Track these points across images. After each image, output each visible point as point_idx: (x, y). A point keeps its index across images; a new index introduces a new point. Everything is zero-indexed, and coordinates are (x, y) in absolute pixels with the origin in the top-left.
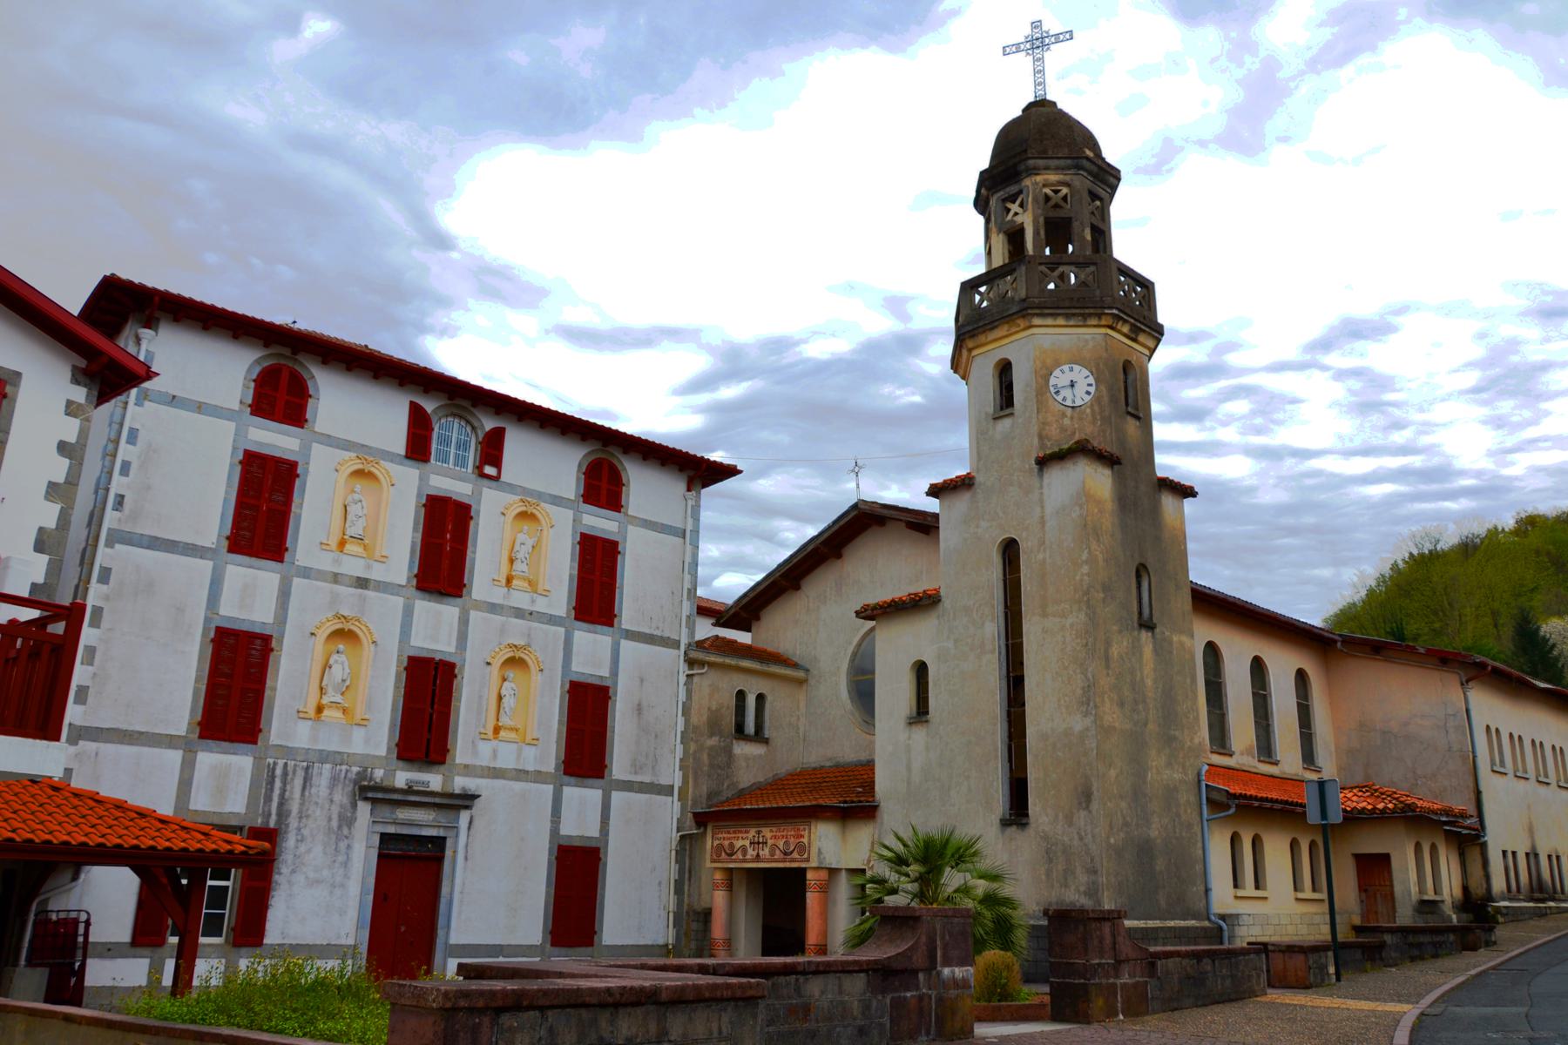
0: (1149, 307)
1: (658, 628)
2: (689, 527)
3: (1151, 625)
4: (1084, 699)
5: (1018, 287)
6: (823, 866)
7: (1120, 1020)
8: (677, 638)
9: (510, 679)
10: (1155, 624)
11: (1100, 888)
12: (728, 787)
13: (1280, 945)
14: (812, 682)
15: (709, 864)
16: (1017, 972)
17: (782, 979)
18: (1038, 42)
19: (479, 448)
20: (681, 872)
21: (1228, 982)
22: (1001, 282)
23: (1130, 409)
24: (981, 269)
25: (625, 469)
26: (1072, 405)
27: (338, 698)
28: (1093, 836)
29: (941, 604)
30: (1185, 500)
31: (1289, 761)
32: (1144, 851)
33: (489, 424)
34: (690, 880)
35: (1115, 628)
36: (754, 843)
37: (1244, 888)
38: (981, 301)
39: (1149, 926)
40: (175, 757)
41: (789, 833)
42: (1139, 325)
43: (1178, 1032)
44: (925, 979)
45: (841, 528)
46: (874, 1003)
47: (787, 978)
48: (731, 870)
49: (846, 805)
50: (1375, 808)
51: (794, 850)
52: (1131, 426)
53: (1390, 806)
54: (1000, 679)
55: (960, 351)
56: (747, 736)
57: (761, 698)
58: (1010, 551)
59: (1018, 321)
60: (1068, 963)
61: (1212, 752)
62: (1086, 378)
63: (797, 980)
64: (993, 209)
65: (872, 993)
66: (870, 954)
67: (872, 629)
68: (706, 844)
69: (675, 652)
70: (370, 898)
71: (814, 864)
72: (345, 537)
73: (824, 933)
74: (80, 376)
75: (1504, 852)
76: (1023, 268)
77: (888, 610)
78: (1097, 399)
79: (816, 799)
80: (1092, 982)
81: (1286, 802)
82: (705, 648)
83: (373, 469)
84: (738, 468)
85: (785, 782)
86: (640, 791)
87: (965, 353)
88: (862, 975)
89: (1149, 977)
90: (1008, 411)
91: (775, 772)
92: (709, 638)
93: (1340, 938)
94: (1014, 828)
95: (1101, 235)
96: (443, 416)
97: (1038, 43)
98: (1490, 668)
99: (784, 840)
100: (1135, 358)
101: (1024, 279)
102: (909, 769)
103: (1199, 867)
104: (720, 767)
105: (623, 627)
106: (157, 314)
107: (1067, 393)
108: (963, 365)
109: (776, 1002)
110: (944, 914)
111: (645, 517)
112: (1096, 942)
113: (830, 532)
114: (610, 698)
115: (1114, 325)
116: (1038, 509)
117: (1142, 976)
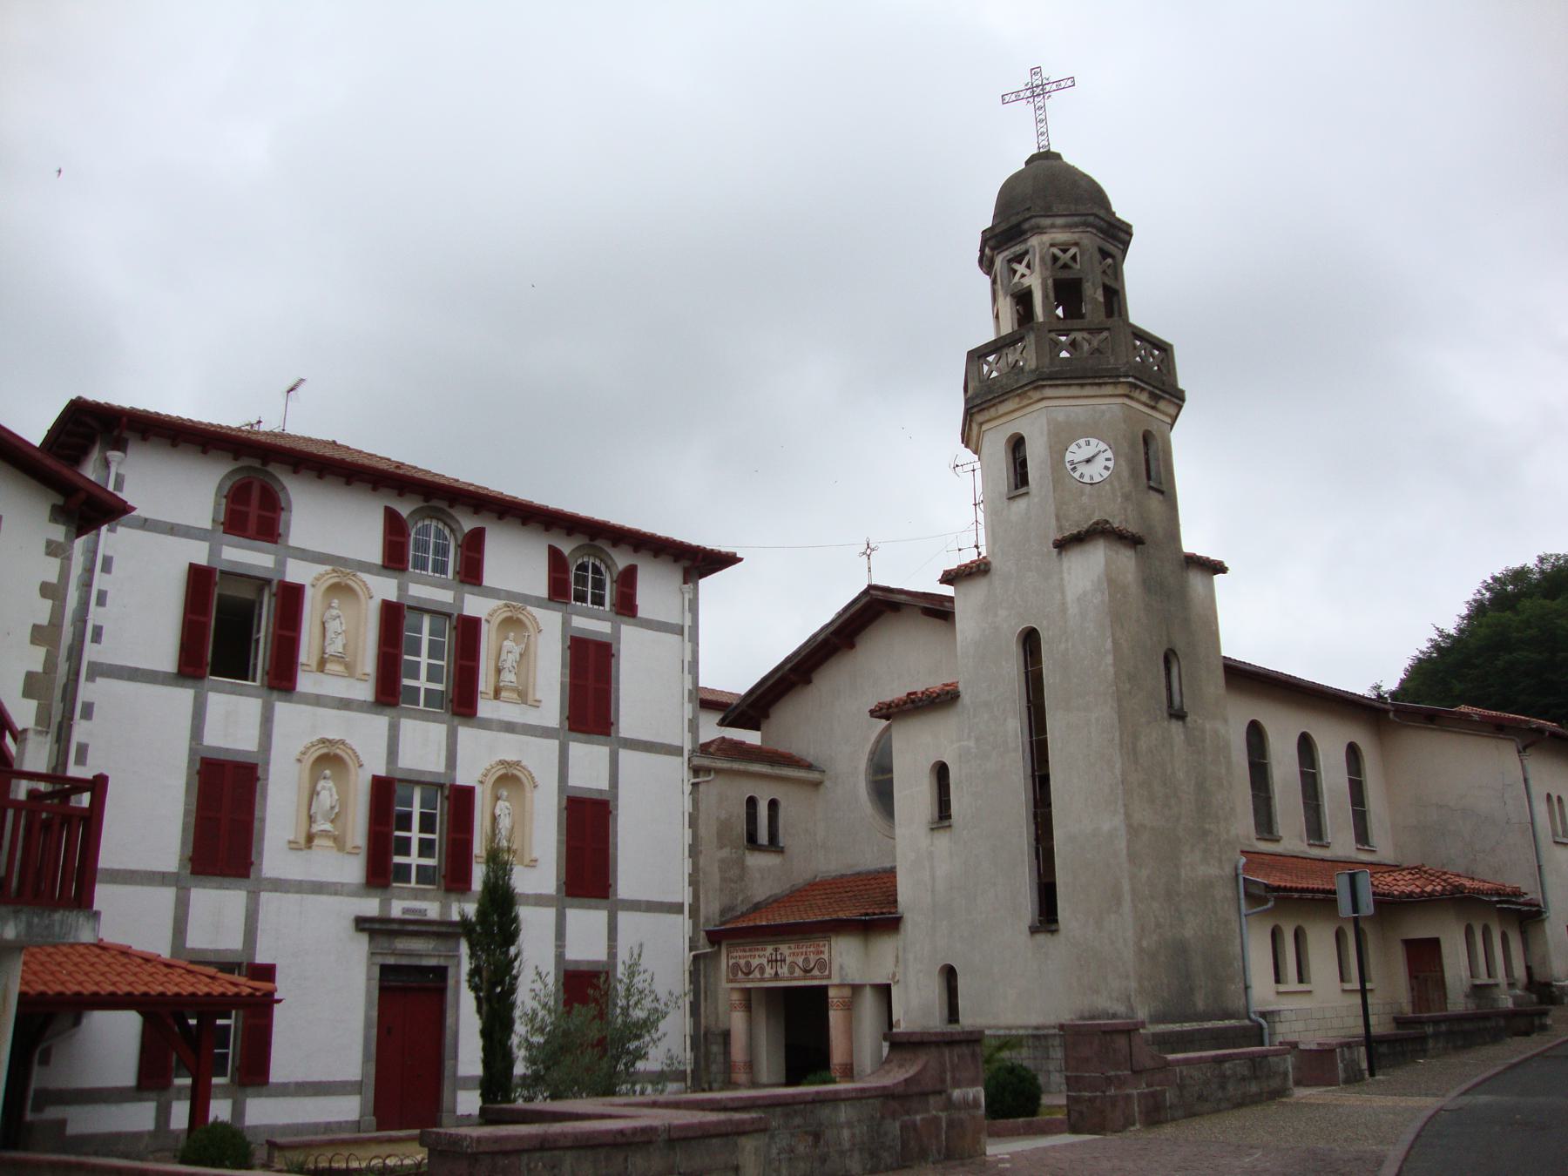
0: (1169, 372)
2: (688, 623)
5: (1027, 357)
6: (846, 982)
8: (680, 744)
9: (504, 797)
12: (742, 902)
14: (827, 783)
15: (725, 985)
18: (1038, 90)
19: (459, 553)
23: (1152, 484)
27: (328, 826)
29: (960, 700)
30: (1215, 577)
31: (1341, 843)
32: (1180, 949)
33: (468, 524)
34: (706, 1000)
36: (772, 961)
39: (1185, 1029)
40: (168, 895)
42: (1157, 392)
45: (852, 615)
48: (748, 990)
49: (867, 918)
50: (1422, 891)
51: (814, 968)
52: (1155, 501)
53: (1438, 888)
55: (970, 425)
57: (773, 805)
58: (1030, 641)
68: (720, 963)
69: (679, 759)
70: (374, 1032)
71: (835, 980)
72: (326, 656)
73: (851, 1053)
74: (59, 514)
78: (1115, 474)
83: (350, 582)
84: (738, 556)
87: (975, 427)
93: (1375, 1030)
95: (1114, 297)
96: (420, 519)
97: (1038, 91)
98: (1547, 734)
99: (803, 957)
100: (1155, 427)
101: (1033, 346)
102: (933, 878)
103: (1238, 964)
105: (621, 735)
106: (126, 434)
114: (610, 812)
116: (1059, 596)
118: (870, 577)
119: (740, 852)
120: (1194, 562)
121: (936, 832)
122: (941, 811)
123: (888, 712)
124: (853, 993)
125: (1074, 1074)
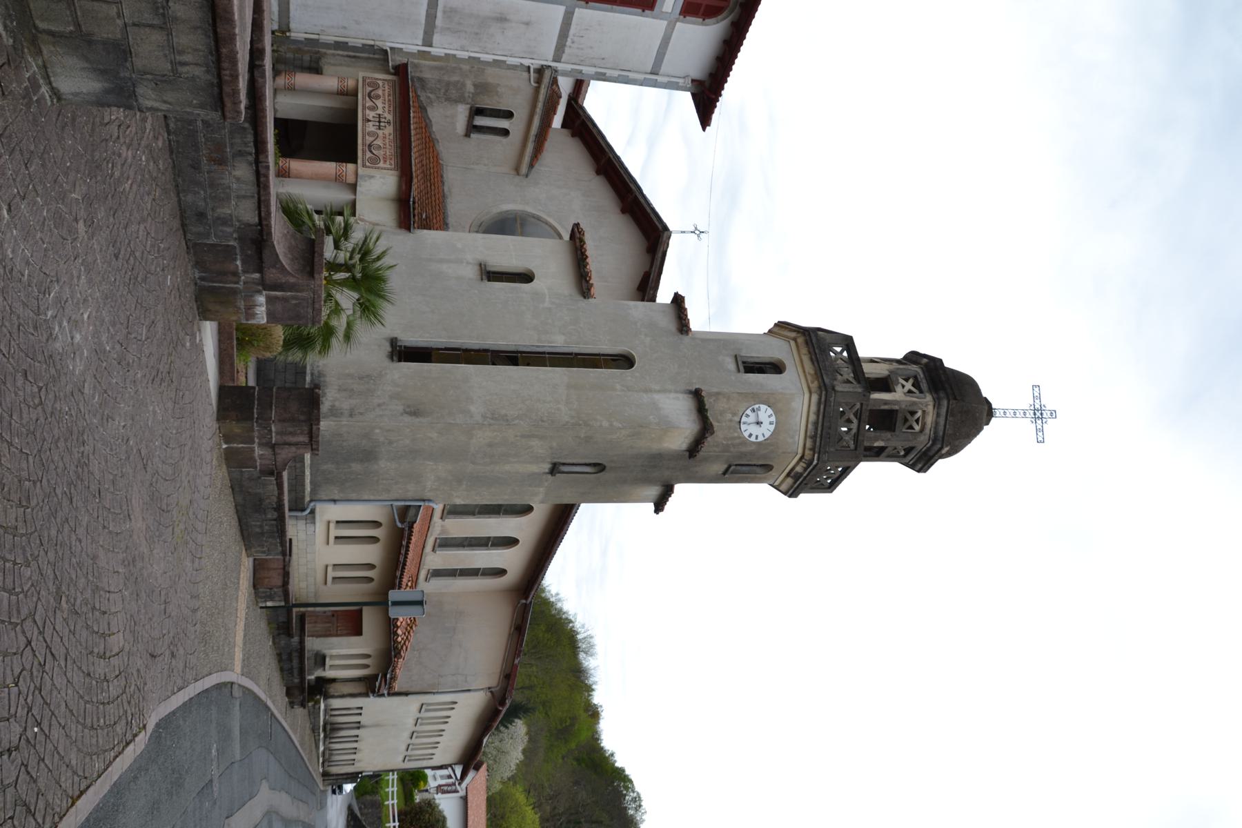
1: (573, 42)
2: (660, 79)
3: (555, 471)
4: (497, 416)
6: (359, 179)
7: (221, 445)
8: (562, 60)
10: (555, 475)
11: (338, 419)
12: (429, 98)
13: (289, 566)
14: (517, 179)
15: (361, 75)
16: (263, 356)
17: (250, 138)
20: (354, 49)
21: (258, 530)
22: (850, 370)
23: (732, 468)
24: (862, 353)
25: (718, 22)
26: (742, 421)
28: (381, 416)
29: (582, 298)
32: (369, 456)
34: (349, 56)
35: (554, 444)
36: (380, 117)
37: (336, 528)
38: (835, 353)
41: (388, 151)
42: (801, 480)
43: (211, 498)
44: (253, 279)
45: (649, 214)
46: (229, 230)
47: (252, 144)
48: (356, 95)
49: (411, 203)
50: (398, 627)
51: (373, 154)
52: (719, 468)
53: (399, 639)
54: (515, 345)
55: (795, 331)
56: (473, 118)
57: (505, 132)
58: (625, 361)
59: (816, 383)
60: (272, 403)
61: (445, 505)
62: (763, 434)
63: (251, 154)
64: (909, 367)
65: (239, 228)
66: (278, 227)
67: (560, 237)
69: (551, 57)
71: (361, 171)
73: (299, 176)
75: (361, 708)
76: (860, 390)
77: (579, 252)
78: (745, 442)
79: (417, 177)
80: (255, 424)
81: (404, 564)
82: (552, 85)
84: (708, 128)
85: (431, 150)
86: (428, 15)
87: (793, 335)
88: (257, 220)
89: (260, 470)
90: (741, 368)
91: (440, 141)
92: (559, 88)
94: (389, 349)
95: (877, 454)
98: (501, 708)
99: (382, 145)
101: (851, 390)
102: (441, 261)
103: (354, 496)
104: (447, 91)
105: (577, 9)
107: (752, 418)
108: (782, 333)
109: (227, 130)
110: (315, 300)
111: (672, 38)
112: (291, 429)
113: (645, 205)
115: (803, 460)
116: (657, 387)
117: (260, 465)
118: (677, 232)
119: (470, 100)
120: (667, 491)
121: (478, 267)
122: (495, 273)
123: (577, 236)
124: (349, 184)
125: (274, 394)
